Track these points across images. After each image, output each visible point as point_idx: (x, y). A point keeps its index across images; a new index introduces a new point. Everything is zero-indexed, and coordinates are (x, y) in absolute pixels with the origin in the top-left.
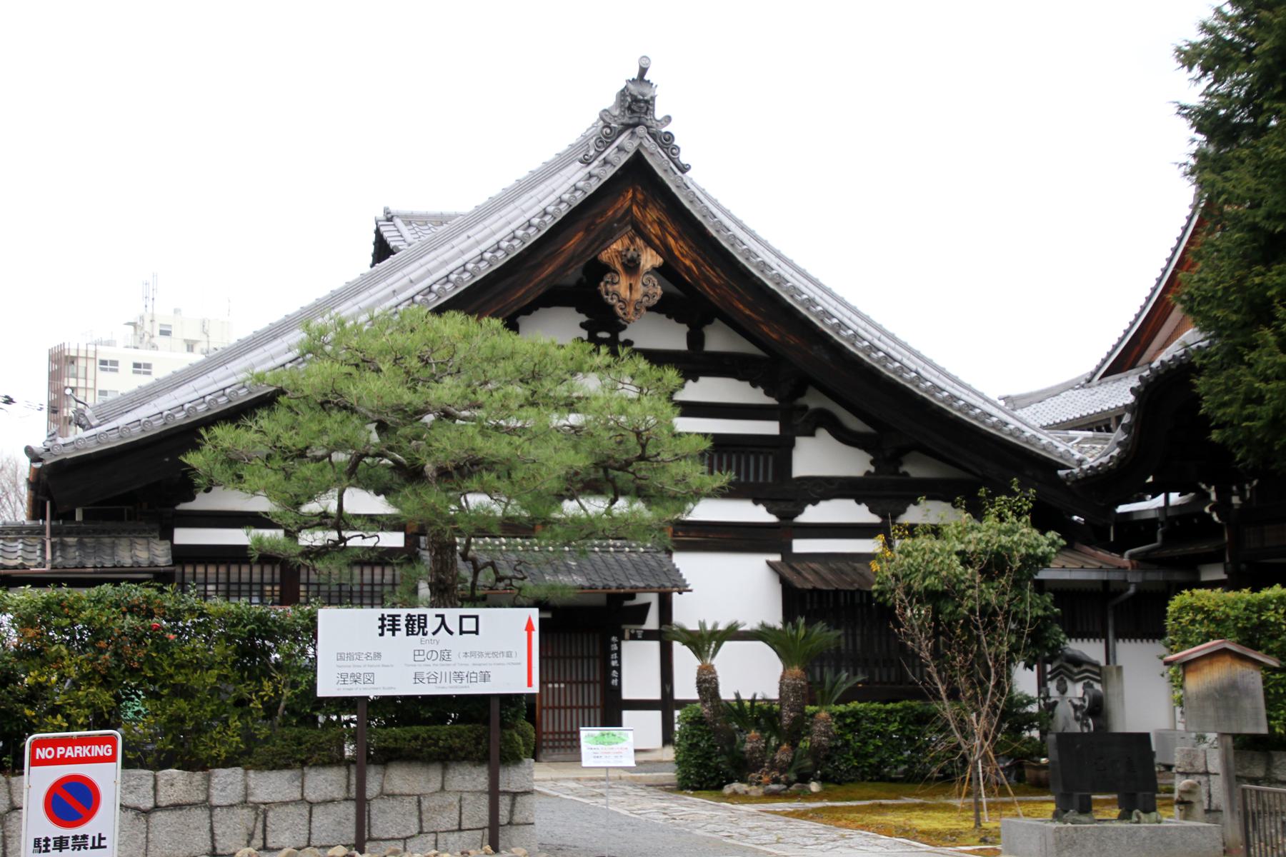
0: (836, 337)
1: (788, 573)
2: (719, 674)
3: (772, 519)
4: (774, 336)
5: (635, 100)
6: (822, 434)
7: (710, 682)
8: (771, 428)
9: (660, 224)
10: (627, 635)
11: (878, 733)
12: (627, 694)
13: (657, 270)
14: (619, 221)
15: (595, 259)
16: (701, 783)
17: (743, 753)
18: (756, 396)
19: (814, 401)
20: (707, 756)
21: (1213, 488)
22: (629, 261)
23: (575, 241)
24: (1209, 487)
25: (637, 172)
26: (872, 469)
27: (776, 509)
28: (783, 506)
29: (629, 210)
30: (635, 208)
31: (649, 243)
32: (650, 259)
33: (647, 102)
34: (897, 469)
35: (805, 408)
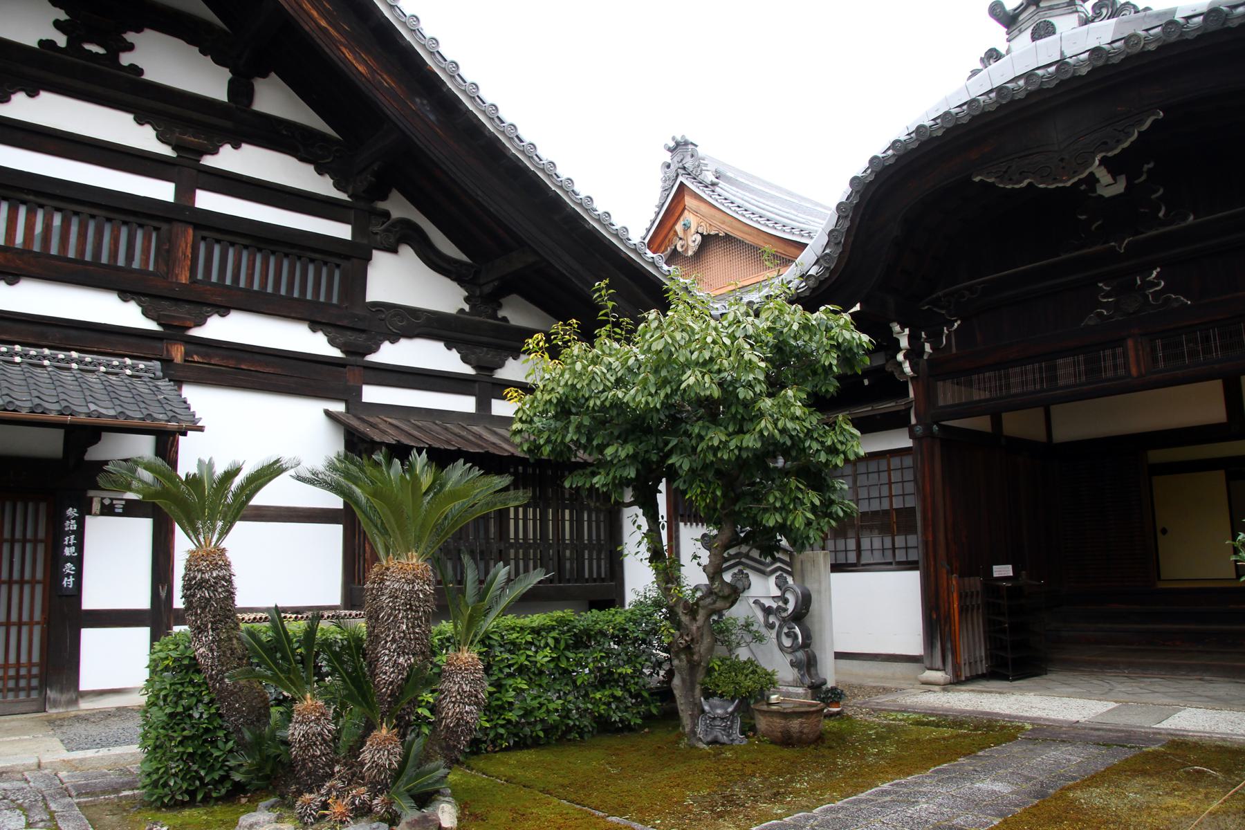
0: (450, 85)
1: (355, 423)
2: (235, 569)
3: (336, 353)
4: (361, 68)
6: (407, 252)
7: (213, 588)
8: (341, 231)
10: (96, 507)
11: (522, 670)
12: (91, 600)
16: (192, 794)
17: (286, 743)
18: (323, 186)
19: (398, 208)
20: (206, 736)
21: (907, 331)
24: (903, 329)
26: (467, 308)
27: (341, 340)
28: (351, 337)
34: (495, 312)
35: (386, 214)
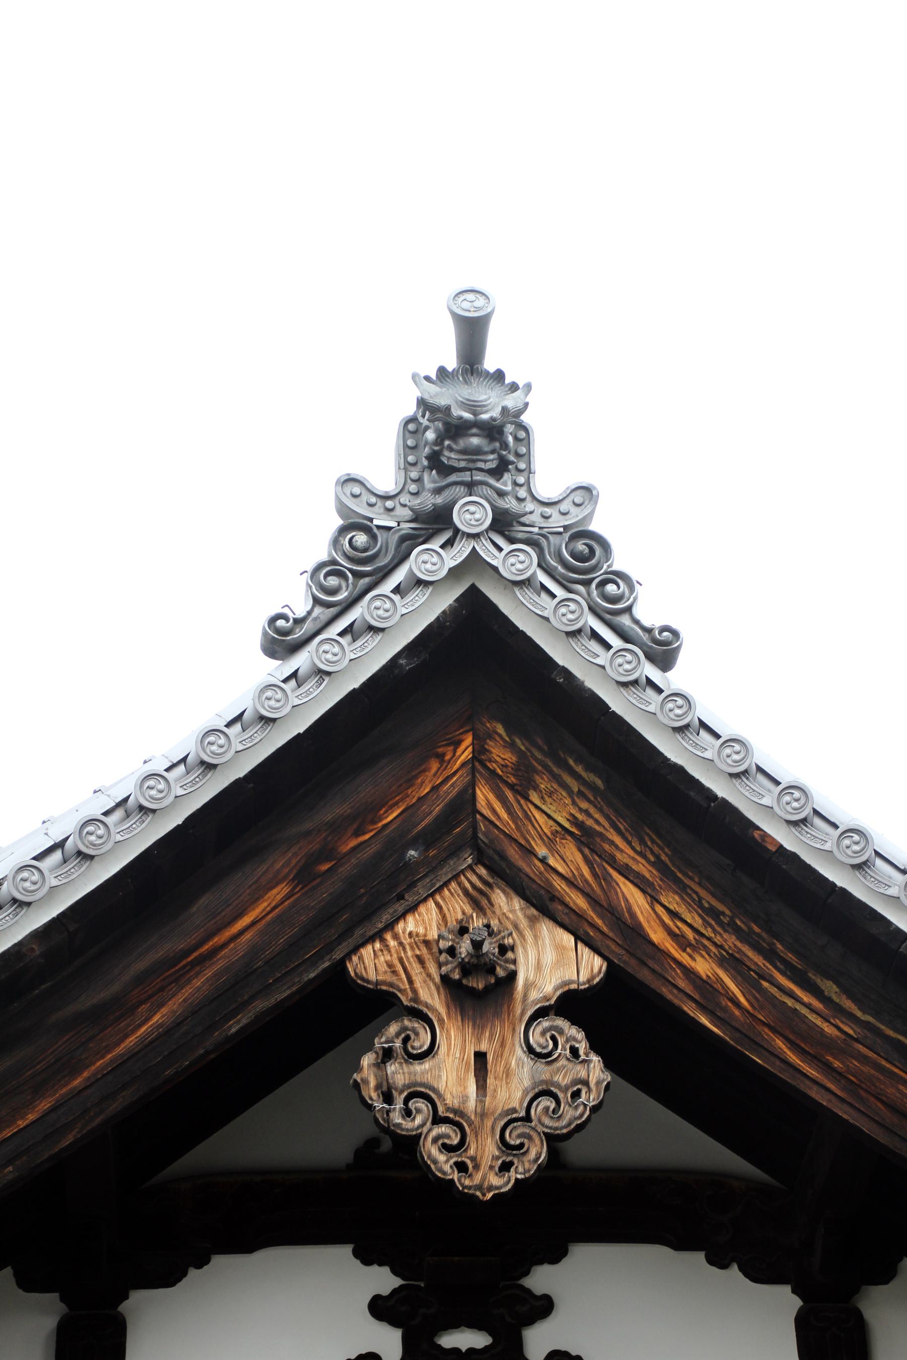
5: (454, 430)
9: (586, 838)
13: (570, 1004)
14: (428, 839)
15: (340, 967)
22: (466, 969)
23: (257, 910)
25: (474, 666)
29: (464, 803)
30: (484, 796)
31: (544, 904)
32: (550, 962)
33: (493, 431)
